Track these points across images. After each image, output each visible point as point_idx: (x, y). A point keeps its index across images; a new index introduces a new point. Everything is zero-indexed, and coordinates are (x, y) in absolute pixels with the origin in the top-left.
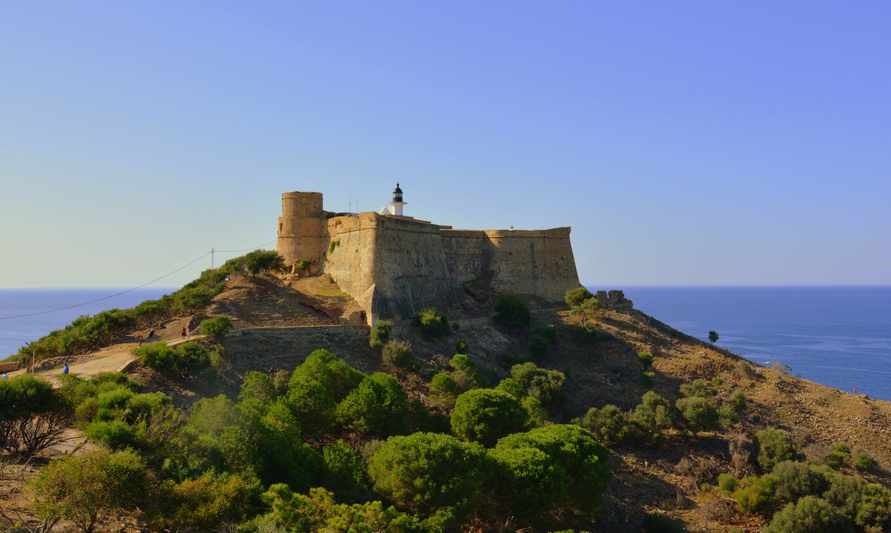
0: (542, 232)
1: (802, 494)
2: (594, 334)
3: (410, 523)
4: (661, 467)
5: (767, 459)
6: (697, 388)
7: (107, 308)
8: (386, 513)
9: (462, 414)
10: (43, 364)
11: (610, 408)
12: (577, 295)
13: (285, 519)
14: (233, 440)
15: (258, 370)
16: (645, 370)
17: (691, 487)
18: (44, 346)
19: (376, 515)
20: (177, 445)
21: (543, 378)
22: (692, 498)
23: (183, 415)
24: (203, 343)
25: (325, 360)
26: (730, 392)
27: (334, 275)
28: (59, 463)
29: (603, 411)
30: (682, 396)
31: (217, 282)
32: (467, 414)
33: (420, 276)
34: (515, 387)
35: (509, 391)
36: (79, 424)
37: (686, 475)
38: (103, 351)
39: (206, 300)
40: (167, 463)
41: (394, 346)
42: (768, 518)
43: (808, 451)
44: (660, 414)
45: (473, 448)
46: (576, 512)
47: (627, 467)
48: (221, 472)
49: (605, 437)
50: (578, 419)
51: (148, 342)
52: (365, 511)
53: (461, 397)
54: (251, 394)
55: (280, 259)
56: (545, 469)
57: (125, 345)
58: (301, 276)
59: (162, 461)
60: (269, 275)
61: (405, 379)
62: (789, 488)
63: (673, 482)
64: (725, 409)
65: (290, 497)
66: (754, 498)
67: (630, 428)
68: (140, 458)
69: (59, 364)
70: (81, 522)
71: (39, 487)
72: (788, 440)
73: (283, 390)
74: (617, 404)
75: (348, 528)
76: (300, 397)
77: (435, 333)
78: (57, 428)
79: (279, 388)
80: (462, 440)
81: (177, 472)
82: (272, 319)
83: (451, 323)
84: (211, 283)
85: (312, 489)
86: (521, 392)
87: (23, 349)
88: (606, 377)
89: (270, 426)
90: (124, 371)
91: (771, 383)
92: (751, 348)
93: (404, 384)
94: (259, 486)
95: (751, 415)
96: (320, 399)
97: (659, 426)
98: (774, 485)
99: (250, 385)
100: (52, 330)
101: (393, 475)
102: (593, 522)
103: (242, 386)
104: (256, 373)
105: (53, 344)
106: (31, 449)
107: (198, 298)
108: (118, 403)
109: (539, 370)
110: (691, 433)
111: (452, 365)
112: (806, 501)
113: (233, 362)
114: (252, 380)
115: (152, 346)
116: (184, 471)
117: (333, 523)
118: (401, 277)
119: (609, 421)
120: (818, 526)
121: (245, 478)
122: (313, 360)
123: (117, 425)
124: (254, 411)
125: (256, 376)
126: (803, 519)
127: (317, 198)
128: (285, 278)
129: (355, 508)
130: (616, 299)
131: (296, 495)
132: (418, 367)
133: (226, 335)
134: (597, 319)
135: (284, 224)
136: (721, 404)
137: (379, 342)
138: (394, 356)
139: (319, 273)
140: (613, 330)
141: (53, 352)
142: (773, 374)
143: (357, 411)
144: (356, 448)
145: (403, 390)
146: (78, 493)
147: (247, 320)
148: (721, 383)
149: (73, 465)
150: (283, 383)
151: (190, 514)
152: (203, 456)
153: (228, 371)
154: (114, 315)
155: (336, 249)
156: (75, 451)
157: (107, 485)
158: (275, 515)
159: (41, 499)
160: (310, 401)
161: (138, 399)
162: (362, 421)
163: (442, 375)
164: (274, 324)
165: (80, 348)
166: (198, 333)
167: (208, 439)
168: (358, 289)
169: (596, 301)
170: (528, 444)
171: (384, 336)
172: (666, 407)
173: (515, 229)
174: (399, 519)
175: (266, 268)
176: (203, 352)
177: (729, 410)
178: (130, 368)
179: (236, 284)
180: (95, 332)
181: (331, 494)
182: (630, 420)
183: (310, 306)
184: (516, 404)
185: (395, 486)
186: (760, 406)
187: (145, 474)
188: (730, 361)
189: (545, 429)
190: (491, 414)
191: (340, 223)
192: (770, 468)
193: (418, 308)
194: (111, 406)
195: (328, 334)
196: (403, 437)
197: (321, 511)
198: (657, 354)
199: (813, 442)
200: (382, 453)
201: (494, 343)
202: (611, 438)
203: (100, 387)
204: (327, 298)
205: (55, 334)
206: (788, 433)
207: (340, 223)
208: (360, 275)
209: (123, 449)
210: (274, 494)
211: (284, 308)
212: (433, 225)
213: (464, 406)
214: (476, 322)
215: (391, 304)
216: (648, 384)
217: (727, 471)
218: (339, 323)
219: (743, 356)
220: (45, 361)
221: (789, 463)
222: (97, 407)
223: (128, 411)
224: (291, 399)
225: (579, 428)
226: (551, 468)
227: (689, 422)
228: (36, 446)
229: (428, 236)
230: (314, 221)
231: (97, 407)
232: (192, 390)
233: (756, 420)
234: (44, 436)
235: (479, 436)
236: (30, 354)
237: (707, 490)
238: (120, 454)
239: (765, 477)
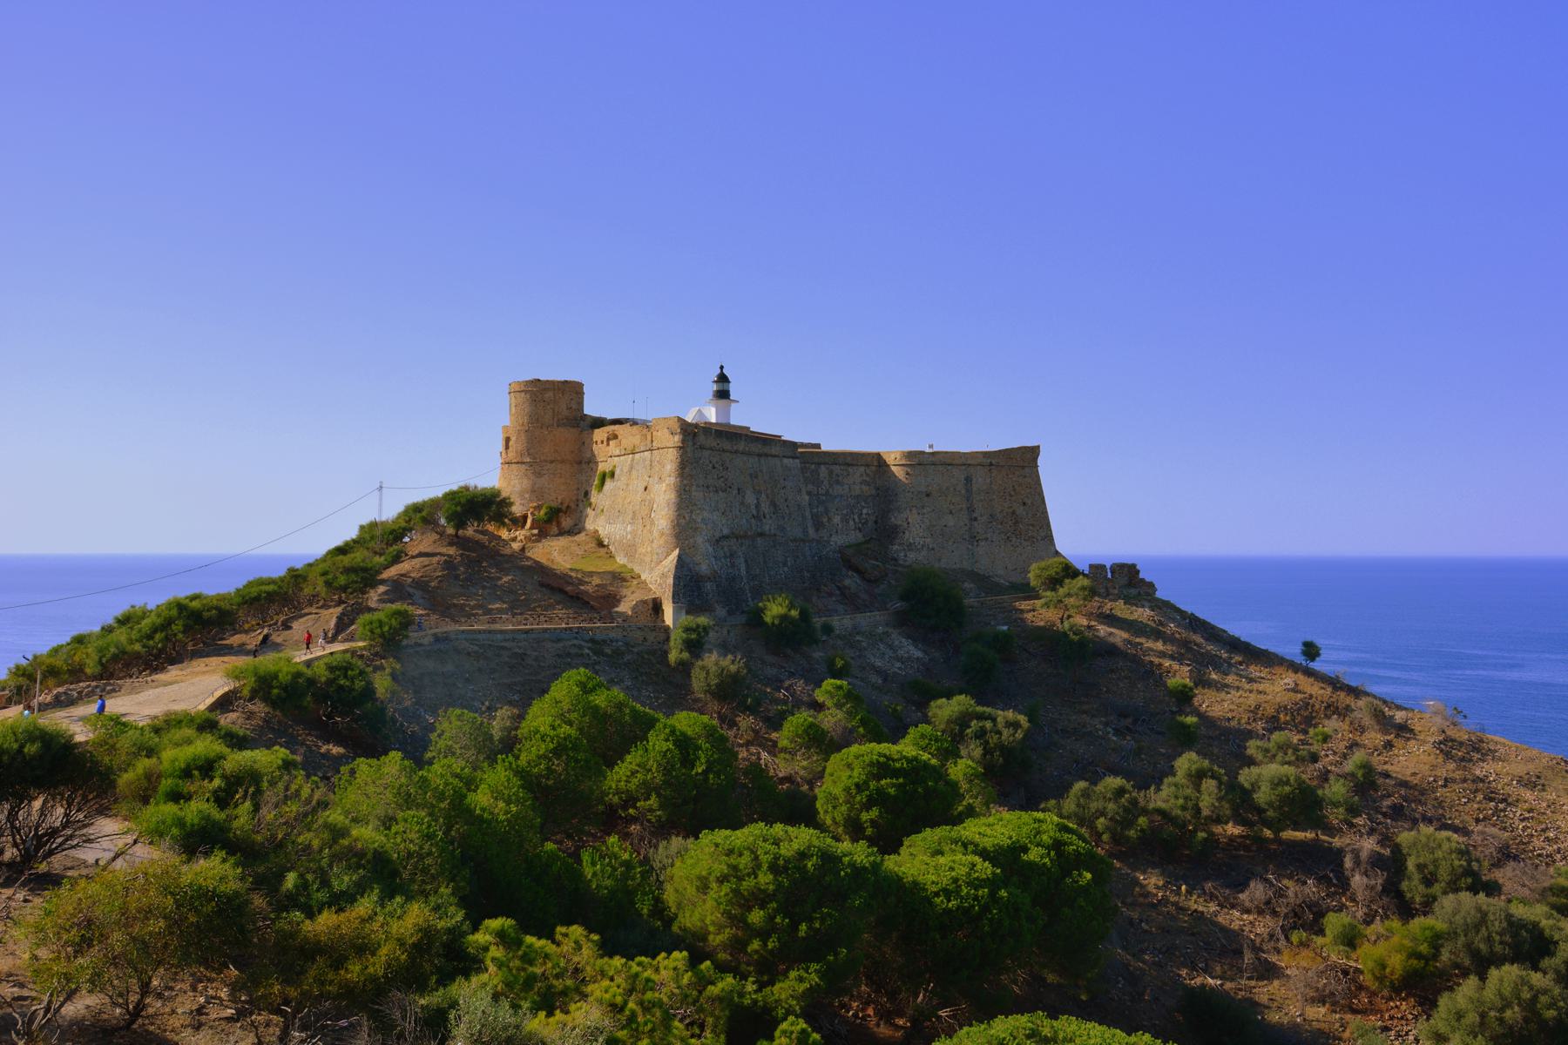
0: (986, 454)
1: (1498, 961)
2: (1083, 643)
3: (741, 995)
4: (1212, 897)
5: (1421, 888)
6: (1280, 747)
7: (182, 592)
8: (696, 974)
9: (837, 790)
10: (57, 696)
11: (1114, 782)
12: (1052, 572)
13: (508, 985)
14: (413, 836)
15: (463, 707)
16: (1181, 712)
17: (1271, 936)
18: (59, 662)
19: (677, 979)
20: (309, 846)
21: (988, 725)
22: (1273, 958)
23: (323, 789)
24: (361, 656)
25: (586, 689)
26: (1345, 756)
27: (603, 533)
28: (83, 883)
29: (1100, 788)
30: (1251, 762)
31: (389, 544)
32: (847, 790)
33: (761, 535)
35: (924, 749)
36: (124, 808)
37: (1260, 912)
38: (173, 672)
39: (366, 578)
40: (291, 879)
41: (713, 662)
42: (1428, 1004)
43: (1505, 876)
45: (859, 853)
46: (1051, 978)
47: (1147, 895)
48: (392, 897)
49: (1105, 837)
50: (1053, 802)
52: (657, 970)
53: (835, 758)
54: (450, 752)
55: (506, 503)
56: (993, 894)
57: (214, 661)
58: (543, 534)
59: (281, 877)
60: (484, 533)
61: (733, 724)
62: (1468, 946)
63: (1235, 926)
64: (1334, 789)
65: (519, 943)
66: (1397, 963)
67: (1152, 822)
68: (239, 870)
69: (88, 695)
70: (121, 995)
71: (39, 929)
72: (1463, 853)
73: (509, 744)
74: (1128, 777)
75: (626, 1003)
76: (539, 757)
77: (790, 640)
78: (81, 816)
79: (501, 740)
80: (837, 839)
81: (309, 896)
82: (488, 612)
83: (818, 621)
84: (377, 546)
85: (560, 929)
86: (946, 750)
87: (18, 668)
88: (1106, 724)
89: (483, 810)
90: (213, 707)
91: (1424, 742)
92: (1382, 673)
93: (731, 733)
94: (462, 922)
95: (1387, 803)
96: (577, 761)
97: (1207, 818)
98: (1436, 940)
99: (447, 735)
100: (75, 633)
101: (710, 903)
102: (1084, 998)
103: (433, 736)
104: (458, 711)
105: (77, 658)
106: (28, 858)
107: (351, 573)
108: (199, 768)
109: (980, 709)
110: (1268, 833)
112: (1506, 976)
113: (415, 692)
115: (267, 661)
116: (321, 896)
117: (598, 994)
118: (726, 537)
119: (1111, 806)
120: (1533, 1026)
121: (436, 908)
122: (563, 689)
123: (197, 809)
124: (456, 781)
125: (459, 718)
126: (1502, 1010)
127: (574, 390)
129: (639, 964)
130: (1125, 580)
131: (530, 939)
132: (758, 703)
134: (1089, 616)
135: (513, 439)
136: (1327, 780)
137: (685, 655)
140: (1119, 636)
141: (76, 673)
142: (1429, 721)
143: (644, 783)
144: (643, 852)
145: (729, 745)
146: (117, 938)
147: (443, 614)
148: (1326, 738)
149: (109, 886)
150: (509, 730)
151: (330, 976)
152: (359, 866)
153: (406, 709)
155: (609, 484)
156: (114, 859)
157: (174, 923)
158: (491, 977)
159: (43, 953)
160: (558, 765)
161: (238, 760)
162: (653, 801)
163: (802, 718)
164: (493, 621)
165: (128, 665)
166: (351, 638)
167: (367, 835)
168: (647, 559)
169: (1086, 582)
170: (959, 848)
171: (695, 645)
174: (720, 985)
175: (480, 519)
176: (362, 673)
177: (1343, 790)
179: (424, 547)
180: (158, 636)
181: (596, 937)
182: (1151, 806)
184: (939, 774)
185: (713, 923)
186: (1404, 784)
187: (248, 902)
188: (1343, 699)
189: (991, 820)
190: (892, 791)
191: (616, 437)
192: (1427, 907)
193: (758, 593)
194: (186, 773)
195: (592, 641)
196: (728, 832)
197: (576, 970)
198: (1202, 682)
199: (1516, 858)
200: (689, 862)
201: (899, 659)
202: (1117, 839)
203: (166, 738)
204: (591, 574)
205: (80, 640)
206: (1461, 839)
207: (616, 437)
208: (651, 532)
209: (207, 854)
210: (488, 938)
211: (511, 592)
212: (785, 442)
213: (841, 775)
214: (864, 620)
215: (709, 586)
216: (1186, 739)
217: (1341, 908)
218: (612, 620)
219: (1368, 689)
220: (61, 690)
221: (1465, 896)
222: (159, 776)
223: (217, 782)
226: (1003, 893)
227: (1265, 811)
228: (37, 850)
229: (777, 461)
230: (567, 434)
231: (159, 776)
232: (338, 743)
233: (1397, 812)
234: (53, 833)
236: (31, 678)
237: (1303, 944)
238: (202, 864)
239: (1418, 923)
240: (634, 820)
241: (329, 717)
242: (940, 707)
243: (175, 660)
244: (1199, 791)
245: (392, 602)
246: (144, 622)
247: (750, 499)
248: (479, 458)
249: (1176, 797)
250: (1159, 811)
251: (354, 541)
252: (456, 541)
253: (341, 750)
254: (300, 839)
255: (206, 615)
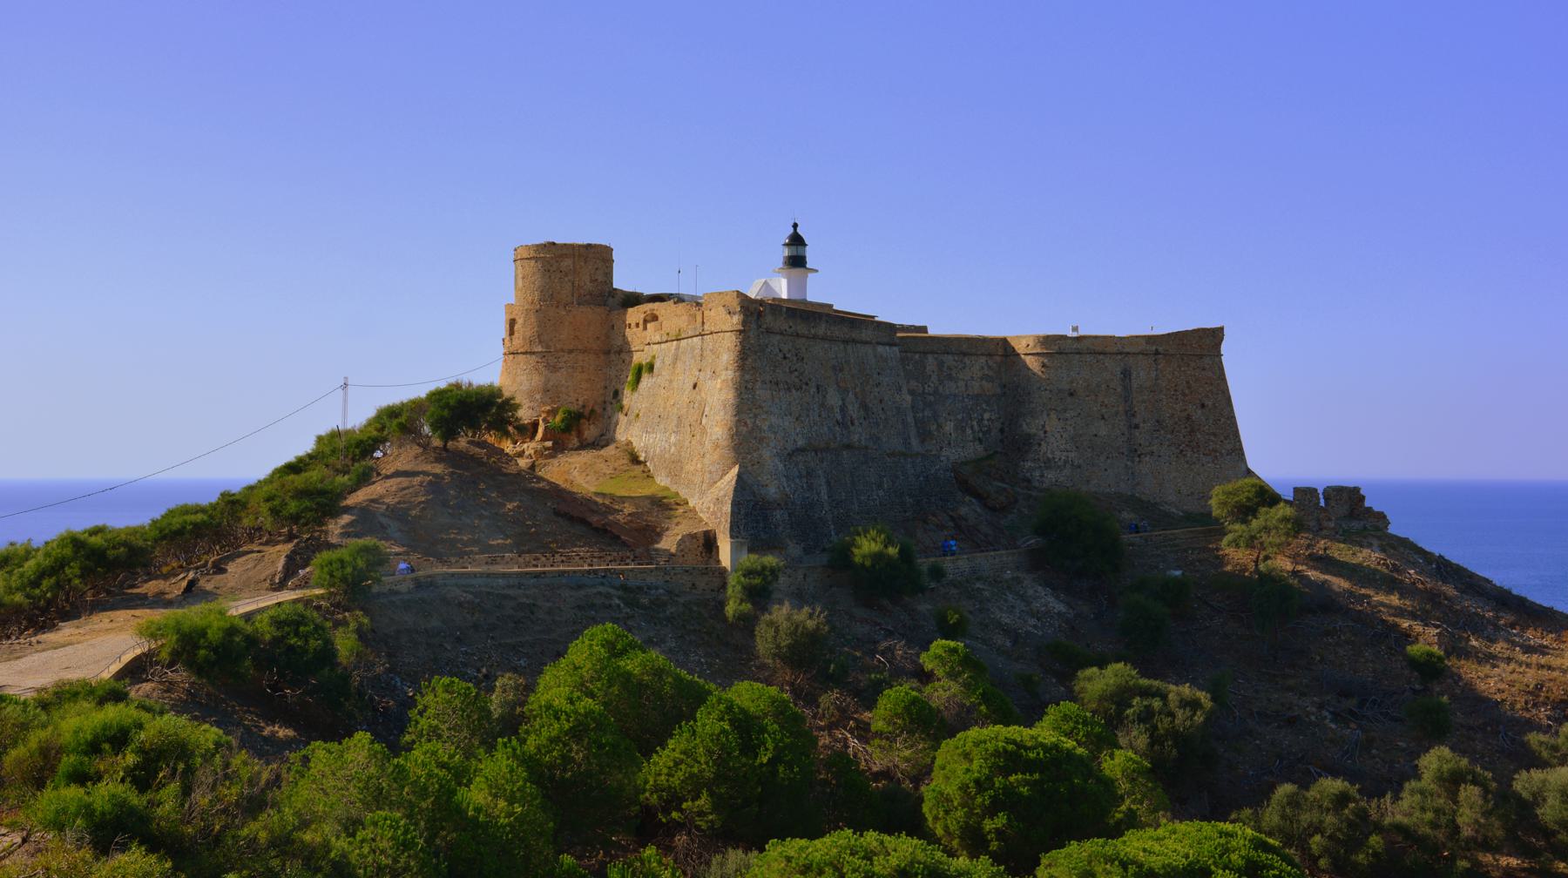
7: (80, 523)
9: (951, 789)
11: (1332, 785)
12: (1242, 497)
14: (384, 844)
21: (1157, 704)
24: (318, 608)
29: (1312, 793)
32: (964, 788)
33: (848, 447)
34: (1085, 723)
35: (1068, 735)
38: (67, 631)
39: (325, 503)
41: (786, 616)
44: (1470, 807)
49: (1323, 863)
50: (1248, 812)
51: (180, 605)
53: (948, 745)
54: (435, 733)
55: (509, 405)
61: (812, 701)
73: (512, 724)
74: (1351, 777)
76: (552, 740)
77: (886, 586)
79: (502, 718)
82: (487, 549)
83: (924, 563)
86: (1098, 736)
88: (1321, 707)
89: (478, 810)
90: (119, 675)
96: (601, 747)
97: (1468, 840)
99: (430, 711)
103: (413, 713)
104: (446, 680)
107: (306, 498)
109: (1144, 682)
111: (929, 666)
113: (389, 655)
114: (437, 700)
115: (194, 614)
118: (802, 450)
119: (1330, 819)
122: (584, 651)
123: (108, 792)
124: (442, 773)
125: (447, 689)
127: (600, 257)
128: (523, 452)
130: (1344, 511)
133: (376, 589)
134: (1295, 558)
135: (520, 321)
137: (746, 607)
138: (785, 642)
139: (603, 440)
140: (1339, 583)
154: (96, 540)
162: (704, 801)
164: (494, 562)
166: (305, 584)
168: (697, 480)
171: (760, 593)
172: (1486, 791)
173: (1082, 332)
175: (474, 426)
178: (136, 670)
180: (46, 583)
182: (1387, 821)
183: (580, 518)
184: (1088, 768)
189: (1160, 832)
190: (1024, 790)
191: (655, 318)
194: (94, 748)
195: (624, 588)
196: (803, 842)
198: (1456, 649)
204: (623, 499)
207: (655, 318)
208: (702, 444)
209: (124, 848)
212: (880, 323)
213: (956, 766)
214: (986, 561)
215: (778, 515)
216: (1434, 729)
223: (131, 759)
224: (532, 743)
225: (1249, 831)
227: (1554, 833)
231: (60, 750)
232: (286, 723)
235: (994, 846)
240: (678, 826)
241: (275, 688)
242: (1090, 679)
243: (69, 615)
244: (1456, 802)
245: (358, 535)
246: (27, 565)
247: (834, 399)
248: (472, 343)
249: (1423, 809)
250: (1399, 828)
251: (310, 456)
252: (444, 455)
253: (290, 733)
254: (245, 832)
255: (111, 553)
